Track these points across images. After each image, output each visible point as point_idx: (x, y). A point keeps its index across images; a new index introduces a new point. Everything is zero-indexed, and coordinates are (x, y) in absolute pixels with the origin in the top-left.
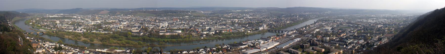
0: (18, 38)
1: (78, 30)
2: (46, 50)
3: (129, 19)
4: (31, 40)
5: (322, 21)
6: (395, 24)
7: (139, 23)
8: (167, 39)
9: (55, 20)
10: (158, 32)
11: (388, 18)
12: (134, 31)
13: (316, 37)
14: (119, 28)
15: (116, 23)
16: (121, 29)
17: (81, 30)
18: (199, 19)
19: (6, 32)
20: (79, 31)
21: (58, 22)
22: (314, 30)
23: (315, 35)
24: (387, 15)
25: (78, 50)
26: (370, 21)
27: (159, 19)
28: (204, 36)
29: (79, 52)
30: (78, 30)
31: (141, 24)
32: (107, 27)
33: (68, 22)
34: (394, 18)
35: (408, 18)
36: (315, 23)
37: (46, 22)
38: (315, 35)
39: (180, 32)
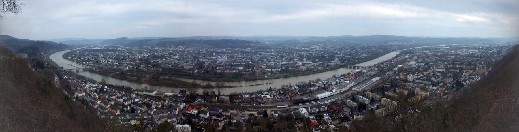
0: (53, 78)
1: (123, 67)
2: (87, 94)
3: (181, 51)
4: (70, 79)
5: (406, 53)
6: (375, 47)
7: (192, 56)
8: (273, 76)
9: (98, 53)
10: (214, 68)
11: (479, 49)
12: (186, 67)
13: (398, 75)
14: (169, 64)
15: (166, 57)
16: (171, 64)
17: (126, 67)
18: (264, 51)
19: (40, 70)
20: (124, 68)
21: (101, 56)
22: (396, 67)
23: (397, 73)
24: (477, 45)
25: (123, 92)
26: (460, 53)
27: (217, 52)
28: (269, 74)
29: (124, 95)
30: (123, 67)
31: (195, 57)
32: (156, 62)
33: (112, 55)
34: (488, 49)
35: (502, 48)
36: (397, 56)
37: (87, 56)
38: (397, 73)
39: (242, 68)
